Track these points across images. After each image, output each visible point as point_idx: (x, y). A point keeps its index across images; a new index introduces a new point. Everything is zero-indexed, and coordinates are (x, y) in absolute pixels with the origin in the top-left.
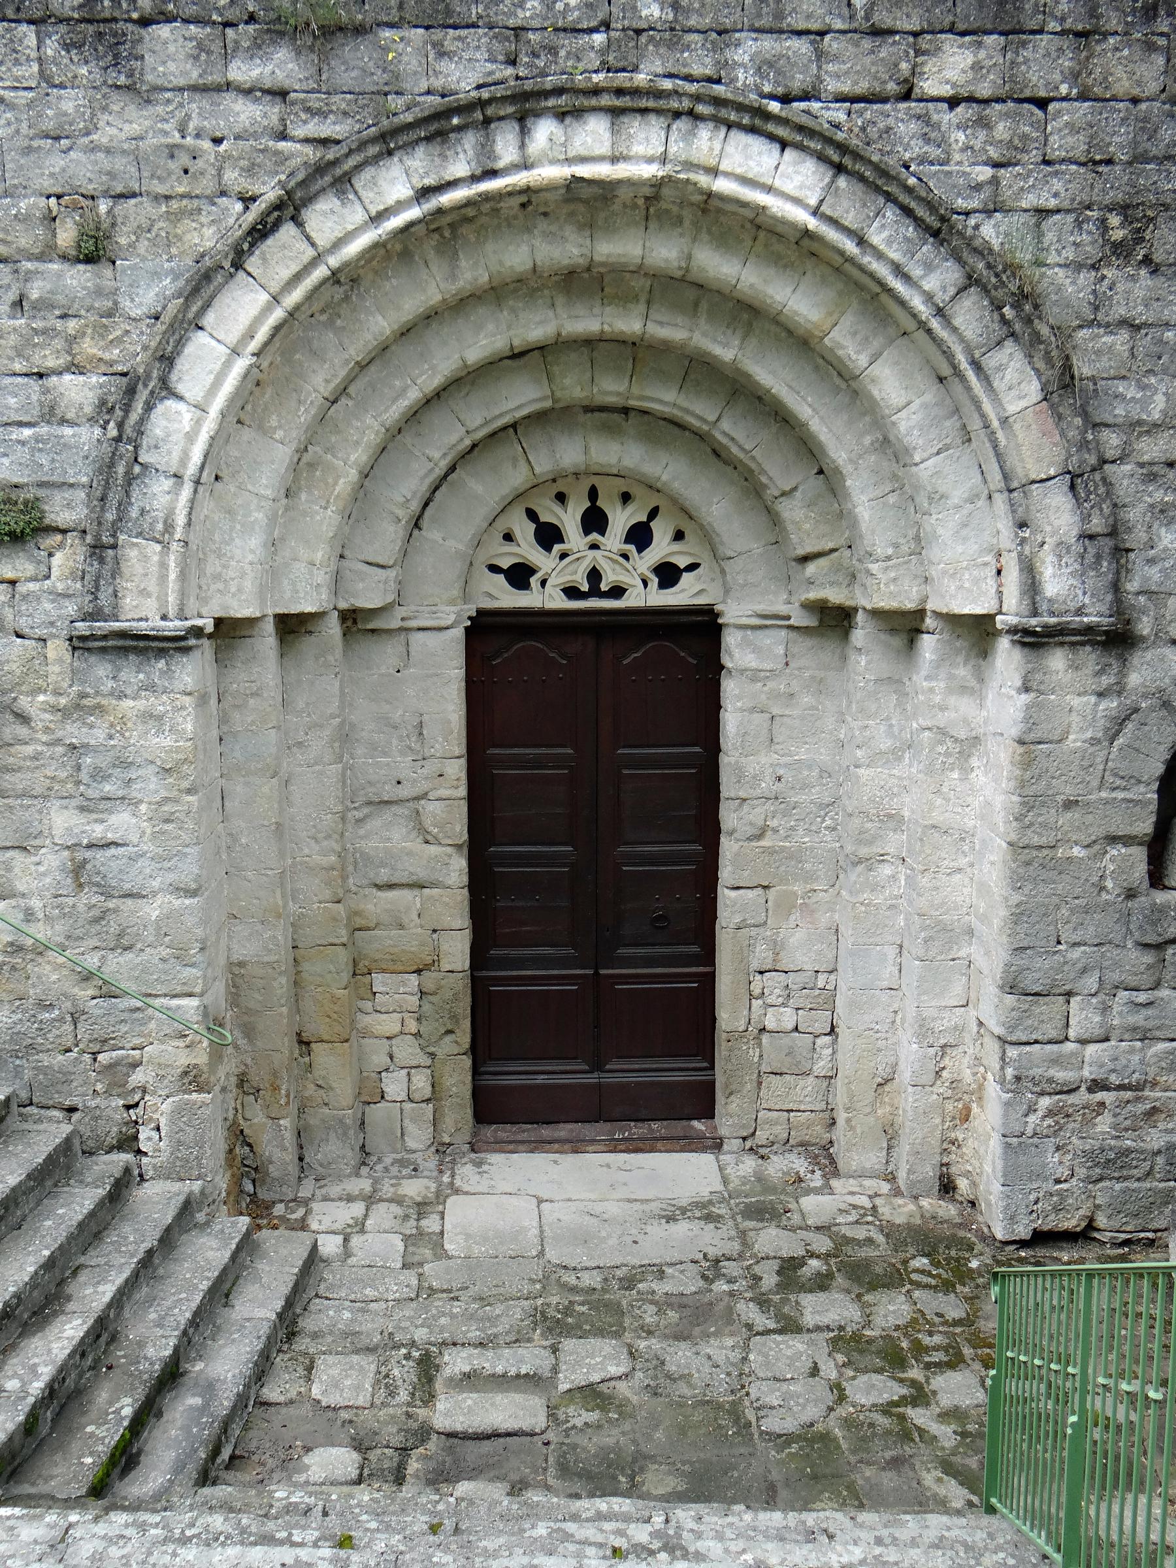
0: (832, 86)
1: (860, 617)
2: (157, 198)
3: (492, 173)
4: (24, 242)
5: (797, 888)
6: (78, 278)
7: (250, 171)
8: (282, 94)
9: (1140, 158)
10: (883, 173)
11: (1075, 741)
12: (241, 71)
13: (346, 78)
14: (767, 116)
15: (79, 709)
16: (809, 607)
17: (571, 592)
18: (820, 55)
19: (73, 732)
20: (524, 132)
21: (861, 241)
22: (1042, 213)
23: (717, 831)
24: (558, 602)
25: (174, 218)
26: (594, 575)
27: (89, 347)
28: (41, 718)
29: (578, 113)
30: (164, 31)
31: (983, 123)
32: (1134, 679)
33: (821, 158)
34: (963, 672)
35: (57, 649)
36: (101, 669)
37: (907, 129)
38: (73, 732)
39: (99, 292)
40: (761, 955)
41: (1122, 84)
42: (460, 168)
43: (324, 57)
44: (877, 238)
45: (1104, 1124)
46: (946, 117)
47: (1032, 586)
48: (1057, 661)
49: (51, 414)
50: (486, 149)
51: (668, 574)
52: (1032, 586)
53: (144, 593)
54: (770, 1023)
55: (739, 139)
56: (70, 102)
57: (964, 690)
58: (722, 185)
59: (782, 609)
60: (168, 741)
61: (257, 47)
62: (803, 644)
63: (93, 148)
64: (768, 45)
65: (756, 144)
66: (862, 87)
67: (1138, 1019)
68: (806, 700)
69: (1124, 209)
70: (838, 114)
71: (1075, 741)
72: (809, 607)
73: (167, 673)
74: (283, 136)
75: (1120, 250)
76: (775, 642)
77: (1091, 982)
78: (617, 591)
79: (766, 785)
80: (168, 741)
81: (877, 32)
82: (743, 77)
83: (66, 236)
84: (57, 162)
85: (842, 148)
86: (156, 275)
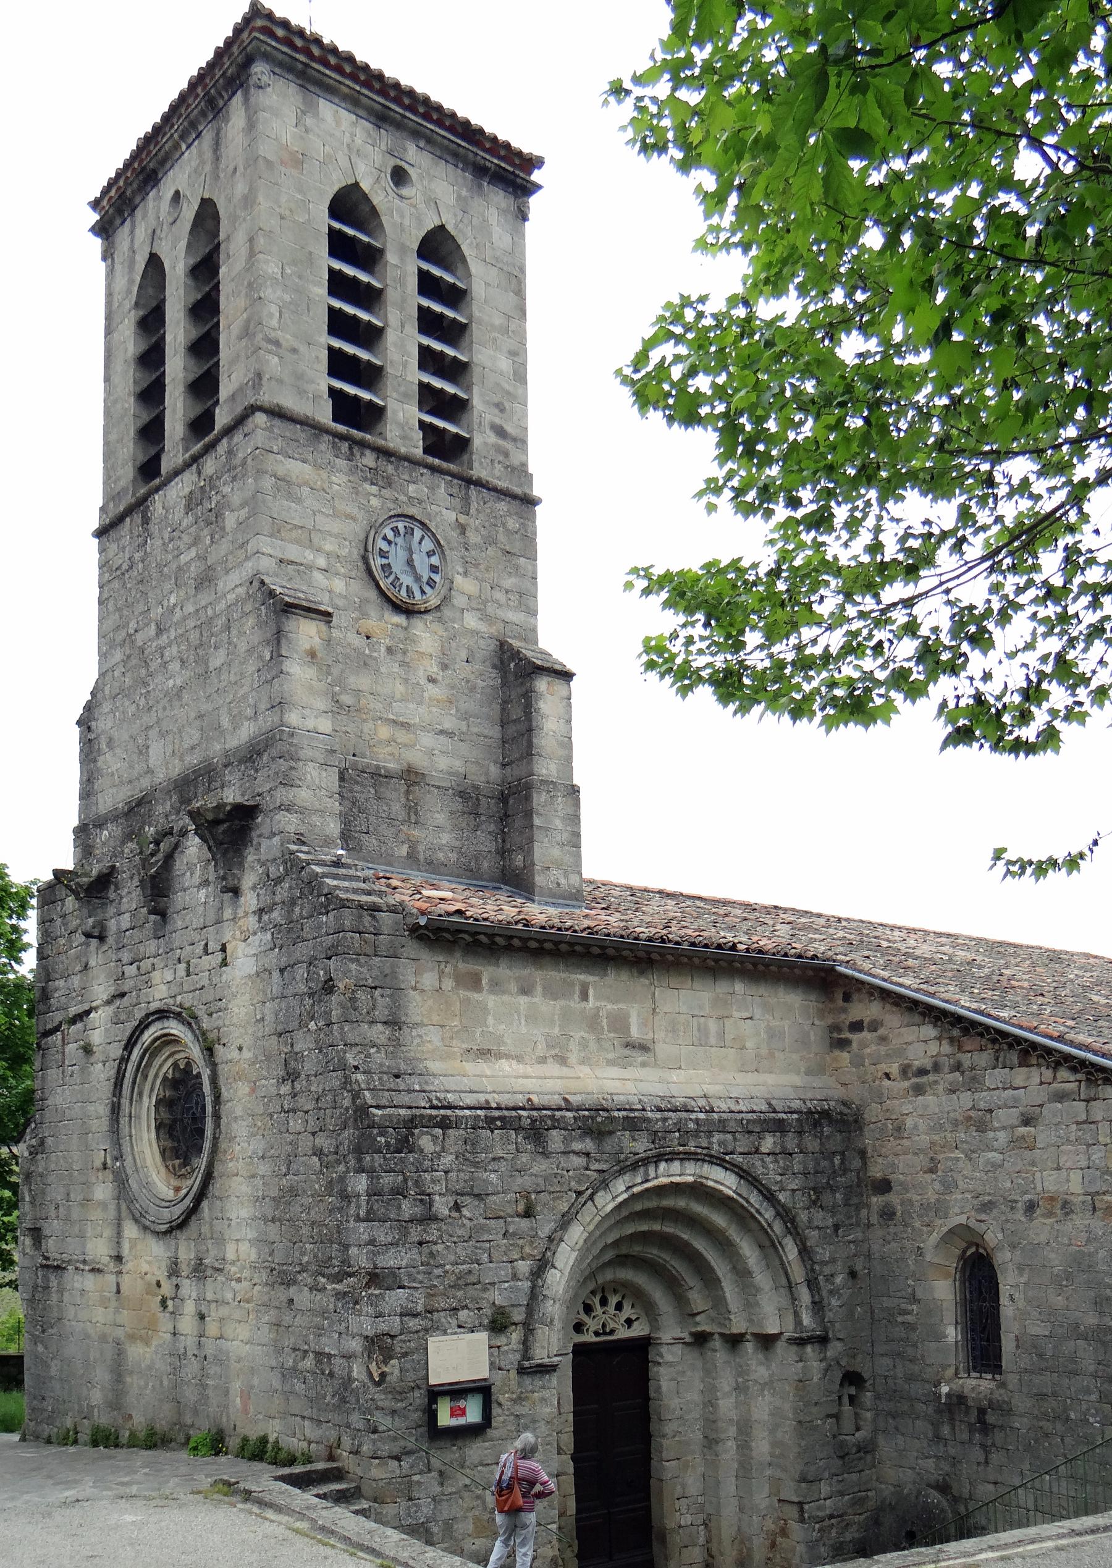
0: (739, 1150)
1: (716, 1337)
2: (551, 1193)
3: (647, 1181)
4: (509, 1211)
5: (689, 1458)
6: (525, 1224)
7: (579, 1182)
8: (588, 1154)
9: (817, 1172)
10: (755, 1178)
11: (815, 1379)
12: (577, 1146)
13: (608, 1148)
14: (724, 1160)
15: (520, 1400)
16: (692, 1334)
17: (597, 1334)
18: (735, 1139)
19: (518, 1410)
20: (657, 1167)
21: (748, 1201)
22: (794, 1191)
23: (650, 1436)
24: (592, 1338)
25: (554, 1199)
26: (604, 1325)
27: (527, 1250)
28: (507, 1404)
29: (671, 1160)
30: (554, 1132)
31: (777, 1161)
32: (828, 1354)
33: (737, 1174)
34: (760, 1356)
35: (513, 1374)
36: (527, 1380)
37: (758, 1163)
38: (518, 1410)
39: (532, 1229)
40: (679, 1491)
41: (810, 1149)
42: (639, 1180)
43: (601, 1141)
44: (752, 1201)
45: (834, 1533)
46: (768, 1159)
47: (798, 1322)
48: (809, 1349)
49: (515, 1277)
50: (646, 1173)
51: (629, 1322)
52: (798, 1322)
53: (543, 1347)
54: (683, 1523)
55: (715, 1168)
56: (524, 1158)
57: (761, 1364)
58: (710, 1183)
59: (682, 1335)
60: (548, 1410)
61: (581, 1138)
62: (687, 1349)
63: (532, 1175)
64: (721, 1136)
65: (719, 1169)
66: (746, 1150)
67: (839, 1487)
68: (689, 1373)
69: (814, 1189)
70: (740, 1159)
71: (815, 1379)
72: (692, 1334)
73: (549, 1380)
74: (587, 1169)
75: (814, 1203)
76: (678, 1349)
77: (826, 1475)
78: (612, 1332)
79: (678, 1413)
80: (548, 1410)
81: (749, 1132)
82: (716, 1147)
83: (521, 1208)
84: (519, 1181)
85: (744, 1171)
86: (549, 1222)
